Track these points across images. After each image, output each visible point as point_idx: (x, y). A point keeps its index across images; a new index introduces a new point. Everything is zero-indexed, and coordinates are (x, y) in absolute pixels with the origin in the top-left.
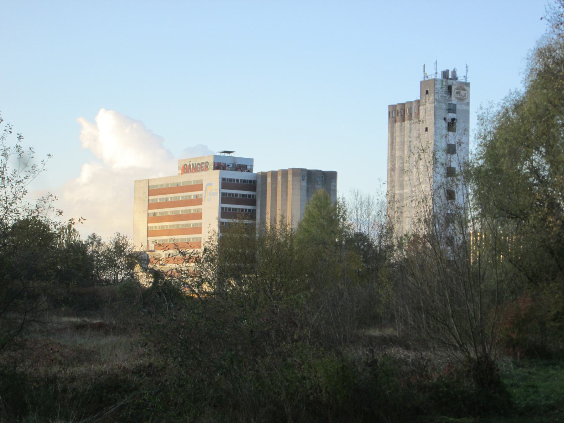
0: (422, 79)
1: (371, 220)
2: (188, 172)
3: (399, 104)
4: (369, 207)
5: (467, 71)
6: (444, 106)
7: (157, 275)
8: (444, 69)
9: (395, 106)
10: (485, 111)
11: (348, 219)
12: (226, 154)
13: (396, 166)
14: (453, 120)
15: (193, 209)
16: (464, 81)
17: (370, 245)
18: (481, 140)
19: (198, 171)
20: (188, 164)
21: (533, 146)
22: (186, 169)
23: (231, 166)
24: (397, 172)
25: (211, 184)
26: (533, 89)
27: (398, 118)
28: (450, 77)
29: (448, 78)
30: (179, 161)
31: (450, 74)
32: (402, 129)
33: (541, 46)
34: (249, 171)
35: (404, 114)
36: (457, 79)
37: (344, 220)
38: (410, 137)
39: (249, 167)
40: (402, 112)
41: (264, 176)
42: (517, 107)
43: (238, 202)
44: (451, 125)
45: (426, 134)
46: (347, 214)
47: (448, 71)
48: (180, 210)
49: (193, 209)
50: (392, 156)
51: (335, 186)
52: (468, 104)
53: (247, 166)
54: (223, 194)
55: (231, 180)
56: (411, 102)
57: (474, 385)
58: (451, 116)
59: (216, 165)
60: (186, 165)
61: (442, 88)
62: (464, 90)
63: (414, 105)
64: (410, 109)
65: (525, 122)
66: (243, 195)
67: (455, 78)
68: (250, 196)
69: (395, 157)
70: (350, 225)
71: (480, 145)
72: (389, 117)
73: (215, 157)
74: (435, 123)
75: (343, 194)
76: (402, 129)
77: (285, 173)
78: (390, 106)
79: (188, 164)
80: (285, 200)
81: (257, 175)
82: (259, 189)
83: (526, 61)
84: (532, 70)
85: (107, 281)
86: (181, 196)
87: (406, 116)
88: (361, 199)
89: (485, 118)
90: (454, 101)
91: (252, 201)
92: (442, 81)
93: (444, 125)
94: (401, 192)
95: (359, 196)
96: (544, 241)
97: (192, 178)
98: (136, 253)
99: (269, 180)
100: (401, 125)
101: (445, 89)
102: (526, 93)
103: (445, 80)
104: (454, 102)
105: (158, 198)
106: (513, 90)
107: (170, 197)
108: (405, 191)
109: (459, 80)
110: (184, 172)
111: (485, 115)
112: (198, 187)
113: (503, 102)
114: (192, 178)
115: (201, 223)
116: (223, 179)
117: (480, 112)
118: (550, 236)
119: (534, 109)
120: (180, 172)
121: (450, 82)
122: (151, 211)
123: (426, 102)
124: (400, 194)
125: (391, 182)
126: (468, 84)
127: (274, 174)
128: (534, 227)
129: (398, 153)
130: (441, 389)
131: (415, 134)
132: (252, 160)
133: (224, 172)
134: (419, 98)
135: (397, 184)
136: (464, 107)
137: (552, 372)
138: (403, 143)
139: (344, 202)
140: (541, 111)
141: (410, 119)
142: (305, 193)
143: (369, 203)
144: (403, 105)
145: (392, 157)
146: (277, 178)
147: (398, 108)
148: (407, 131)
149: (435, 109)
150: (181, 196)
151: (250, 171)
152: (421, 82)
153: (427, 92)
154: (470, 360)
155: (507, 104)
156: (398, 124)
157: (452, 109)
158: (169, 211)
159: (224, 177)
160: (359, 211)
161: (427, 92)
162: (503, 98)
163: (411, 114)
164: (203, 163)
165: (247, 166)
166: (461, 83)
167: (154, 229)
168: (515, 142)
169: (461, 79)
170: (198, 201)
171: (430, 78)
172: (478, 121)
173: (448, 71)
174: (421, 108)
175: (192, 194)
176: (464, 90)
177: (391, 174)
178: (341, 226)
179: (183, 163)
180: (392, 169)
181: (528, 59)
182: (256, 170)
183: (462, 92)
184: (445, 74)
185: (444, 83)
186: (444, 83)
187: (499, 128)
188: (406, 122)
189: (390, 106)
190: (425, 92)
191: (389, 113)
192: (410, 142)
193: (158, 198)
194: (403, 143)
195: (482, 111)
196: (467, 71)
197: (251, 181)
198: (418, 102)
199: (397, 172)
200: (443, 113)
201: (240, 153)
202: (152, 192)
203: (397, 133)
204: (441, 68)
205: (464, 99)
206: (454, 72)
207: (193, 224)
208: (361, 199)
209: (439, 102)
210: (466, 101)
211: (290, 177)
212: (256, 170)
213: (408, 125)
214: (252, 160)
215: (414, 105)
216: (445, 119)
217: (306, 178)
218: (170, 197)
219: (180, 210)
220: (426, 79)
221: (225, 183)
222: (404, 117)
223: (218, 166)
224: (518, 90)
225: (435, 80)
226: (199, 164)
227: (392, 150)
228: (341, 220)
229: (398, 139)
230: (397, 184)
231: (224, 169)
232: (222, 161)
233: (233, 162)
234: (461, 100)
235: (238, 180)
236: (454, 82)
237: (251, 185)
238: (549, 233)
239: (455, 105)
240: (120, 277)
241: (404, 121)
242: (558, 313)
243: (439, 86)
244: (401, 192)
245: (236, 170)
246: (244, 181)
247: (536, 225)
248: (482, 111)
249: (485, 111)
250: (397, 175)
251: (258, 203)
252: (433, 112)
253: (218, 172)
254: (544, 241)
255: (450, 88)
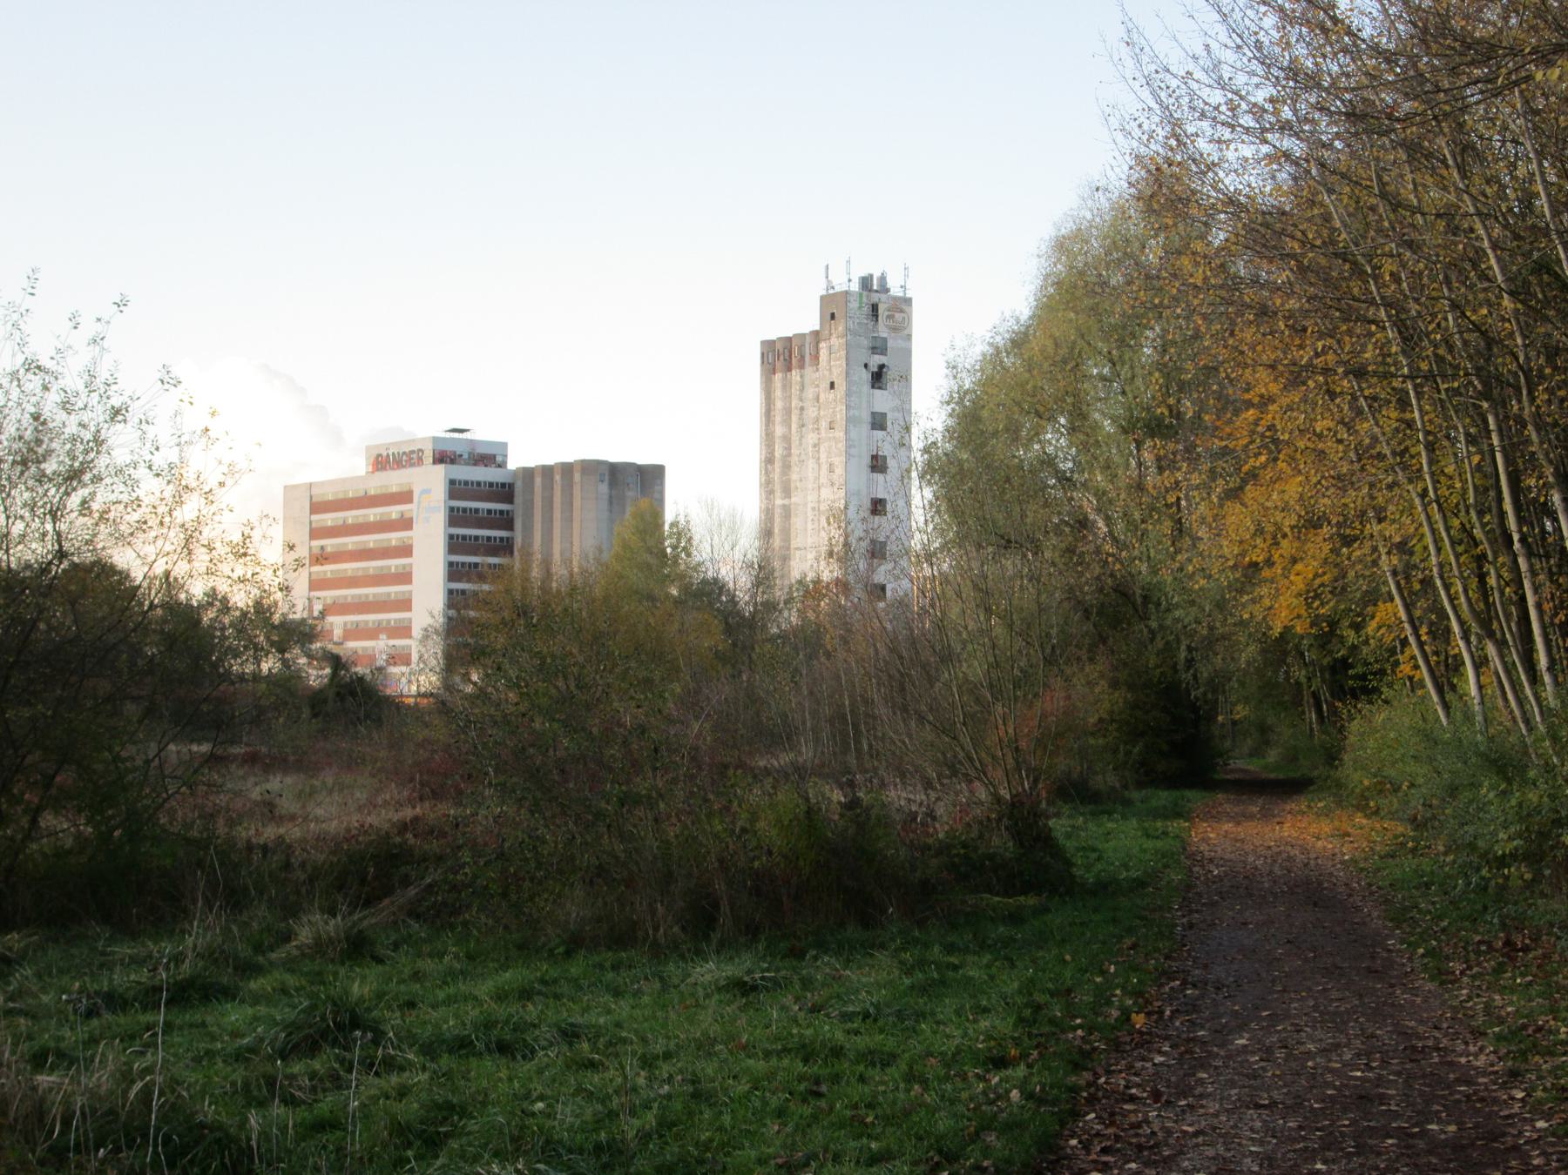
0: (824, 293)
1: (738, 555)
2: (384, 469)
3: (780, 339)
4: (733, 530)
5: (907, 276)
6: (866, 343)
7: (337, 662)
8: (864, 274)
9: (774, 342)
10: (961, 353)
11: (695, 553)
12: (456, 435)
13: (777, 454)
14: (882, 367)
15: (394, 538)
16: (901, 294)
17: (733, 600)
18: (953, 405)
19: (404, 467)
20: (385, 454)
21: (1044, 415)
22: (381, 463)
23: (466, 456)
24: (778, 465)
25: (428, 491)
26: (1047, 309)
27: (779, 365)
28: (875, 288)
29: (871, 290)
30: (368, 448)
31: (875, 282)
32: (786, 386)
33: (1063, 231)
34: (500, 466)
35: (790, 357)
36: (887, 291)
37: (689, 555)
38: (801, 400)
39: (499, 459)
40: (787, 354)
41: (528, 474)
42: (1019, 342)
43: (480, 524)
44: (878, 378)
45: (831, 395)
46: (694, 543)
47: (871, 276)
48: (371, 540)
49: (394, 538)
50: (767, 435)
51: (662, 492)
52: (909, 337)
53: (495, 456)
54: (452, 509)
55: (466, 483)
56: (803, 336)
57: (1011, 844)
58: (877, 360)
59: (437, 456)
60: (380, 455)
61: (860, 308)
62: (902, 311)
63: (808, 339)
64: (801, 347)
65: (1035, 372)
66: (489, 511)
67: (884, 289)
68: (502, 512)
69: (773, 437)
70: (699, 564)
71: (951, 415)
72: (763, 362)
73: (435, 440)
74: (847, 373)
75: (686, 508)
76: (786, 386)
77: (567, 469)
78: (763, 343)
79: (385, 454)
80: (568, 520)
81: (516, 473)
82: (518, 499)
83: (1035, 261)
84: (1047, 277)
85: (242, 678)
86: (372, 514)
87: (794, 361)
88: (719, 515)
89: (960, 366)
90: (883, 332)
91: (506, 522)
92: (861, 295)
93: (866, 376)
94: (786, 502)
95: (715, 512)
96: (1071, 590)
97: (394, 480)
98: (293, 621)
99: (538, 481)
100: (785, 379)
101: (866, 309)
102: (1030, 318)
103: (865, 293)
104: (884, 335)
105: (329, 519)
106: (1008, 314)
107: (351, 516)
108: (793, 499)
109: (891, 293)
110: (378, 470)
111: (959, 360)
112: (405, 497)
113: (990, 334)
114: (394, 480)
115: (411, 565)
116: (452, 482)
117: (951, 355)
118: (1083, 579)
119: (1050, 350)
120: (370, 469)
121: (875, 298)
122: (317, 543)
123: (831, 334)
124: (784, 506)
125: (768, 488)
126: (908, 301)
127: (547, 471)
128: (1054, 564)
129: (779, 430)
130: (954, 852)
131: (810, 393)
132: (504, 445)
133: (454, 467)
134: (817, 328)
135: (778, 487)
136: (901, 344)
137: (1110, 825)
138: (788, 411)
139: (688, 522)
140: (1063, 351)
141: (802, 367)
142: (604, 505)
143: (734, 523)
144: (789, 339)
145: (768, 438)
146: (552, 479)
147: (779, 346)
148: (795, 390)
149: (848, 347)
150: (372, 514)
151: (502, 465)
152: (822, 298)
153: (833, 316)
154: (998, 799)
155: (998, 339)
156: (778, 376)
157: (879, 348)
158: (350, 542)
159: (453, 476)
160: (716, 537)
161: (833, 316)
162: (990, 327)
163: (802, 357)
164: (413, 452)
165: (495, 456)
166: (895, 299)
167: (322, 576)
168: (1016, 409)
169: (895, 291)
170: (406, 523)
171: (838, 289)
172: (947, 371)
173: (871, 276)
174: (822, 345)
175: (394, 511)
176: (902, 311)
177: (766, 470)
178: (682, 567)
179: (376, 452)
180: (769, 460)
181: (1039, 256)
182: (513, 463)
183: (898, 316)
184: (866, 282)
185: (864, 300)
186: (864, 300)
187: (979, 383)
188: (794, 372)
189: (763, 343)
190: (829, 317)
191: (763, 354)
192: (802, 409)
193: (329, 519)
194: (788, 411)
195: (955, 352)
196: (907, 276)
197: (503, 485)
198: (816, 334)
199: (778, 465)
200: (863, 355)
201: (483, 432)
202: (317, 507)
203: (778, 393)
204: (858, 273)
205: (902, 328)
206: (883, 279)
207: (396, 567)
208: (719, 515)
209: (854, 334)
210: (906, 332)
211: (577, 477)
212: (513, 463)
213: (798, 378)
214: (504, 445)
215: (808, 339)
216: (866, 366)
217: (607, 478)
218: (351, 516)
219: (371, 540)
220: (831, 292)
221: (456, 489)
222: (790, 362)
223: (441, 458)
224: (1017, 313)
225: (847, 293)
226: (404, 453)
227: (767, 425)
228: (683, 555)
229: (779, 404)
230: (778, 487)
231: (453, 461)
232: (449, 448)
233: (468, 449)
234: (895, 329)
235: (479, 484)
236: (883, 297)
237: (505, 492)
238: (1081, 574)
239: (885, 340)
240: (265, 667)
241: (789, 369)
242: (1101, 720)
243: (854, 305)
244: (786, 502)
245: (475, 465)
246: (491, 485)
247: (1057, 560)
248: (955, 352)
249: (961, 353)
250: (777, 470)
251: (518, 524)
252: (843, 353)
253: (441, 468)
254: (1071, 590)
255: (875, 308)
